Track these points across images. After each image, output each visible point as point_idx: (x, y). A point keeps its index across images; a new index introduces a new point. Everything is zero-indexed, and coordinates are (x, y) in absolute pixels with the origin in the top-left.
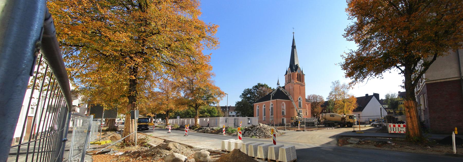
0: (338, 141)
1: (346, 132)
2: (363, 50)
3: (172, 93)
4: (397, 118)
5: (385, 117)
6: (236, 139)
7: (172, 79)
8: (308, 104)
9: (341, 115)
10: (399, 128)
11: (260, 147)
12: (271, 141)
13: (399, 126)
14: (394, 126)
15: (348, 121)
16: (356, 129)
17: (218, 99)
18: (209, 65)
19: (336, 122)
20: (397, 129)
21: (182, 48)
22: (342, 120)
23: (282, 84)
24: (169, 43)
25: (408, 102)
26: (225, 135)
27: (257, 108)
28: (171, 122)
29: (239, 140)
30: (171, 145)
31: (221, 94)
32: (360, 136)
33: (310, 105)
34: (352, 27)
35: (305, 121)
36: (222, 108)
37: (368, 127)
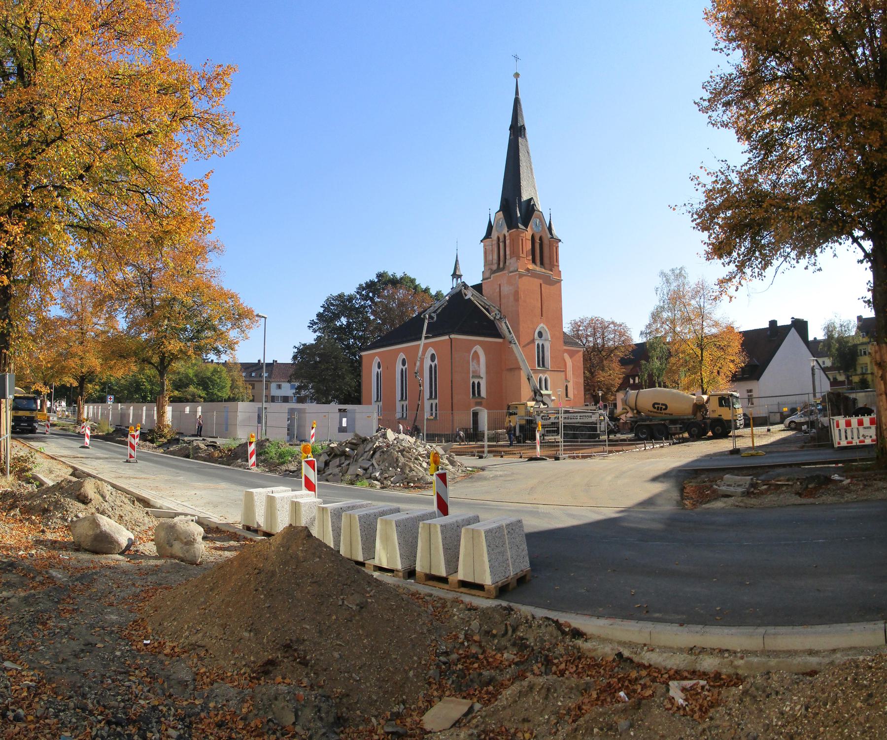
0: (682, 490)
1: (710, 457)
2: (761, 167)
4: (855, 399)
5: (824, 397)
6: (296, 487)
7: (92, 276)
8: (572, 354)
9: (694, 396)
10: (861, 428)
11: (387, 523)
12: (430, 502)
13: (860, 423)
14: (848, 424)
15: (716, 415)
16: (742, 444)
17: (233, 334)
18: (203, 214)
19: (674, 421)
20: (855, 431)
21: (121, 170)
22: (694, 413)
23: (473, 275)
24: (87, 159)
25: (880, 349)
26: (254, 468)
27: (375, 370)
28: (91, 415)
29: (305, 491)
30: (89, 488)
31: (241, 316)
32: (756, 469)
33: (579, 357)
34: (728, 81)
35: (562, 421)
36: (256, 367)
37: (778, 433)
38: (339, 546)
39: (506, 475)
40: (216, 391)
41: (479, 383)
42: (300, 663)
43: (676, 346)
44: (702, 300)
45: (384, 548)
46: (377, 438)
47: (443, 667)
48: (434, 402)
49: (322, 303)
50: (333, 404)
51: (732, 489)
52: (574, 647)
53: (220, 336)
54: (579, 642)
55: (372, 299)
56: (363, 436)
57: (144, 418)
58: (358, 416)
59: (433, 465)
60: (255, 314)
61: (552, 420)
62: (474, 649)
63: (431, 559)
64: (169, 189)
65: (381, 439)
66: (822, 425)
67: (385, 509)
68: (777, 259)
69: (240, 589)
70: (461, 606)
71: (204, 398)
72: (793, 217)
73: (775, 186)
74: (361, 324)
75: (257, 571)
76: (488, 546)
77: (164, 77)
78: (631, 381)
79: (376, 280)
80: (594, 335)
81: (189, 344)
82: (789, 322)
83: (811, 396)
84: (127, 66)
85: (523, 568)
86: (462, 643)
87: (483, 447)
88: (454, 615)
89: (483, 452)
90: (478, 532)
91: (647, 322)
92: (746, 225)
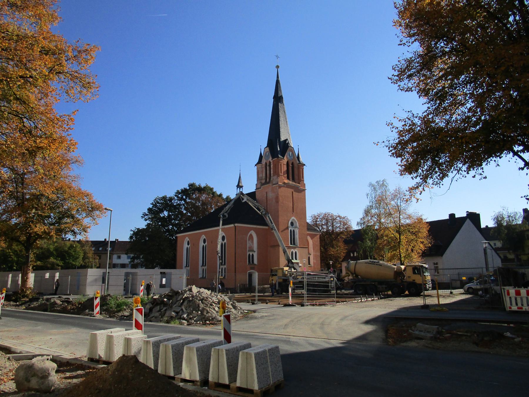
0: (386, 331)
2: (437, 112)
5: (495, 271)
6: (128, 327)
8: (312, 237)
11: (190, 349)
12: (219, 334)
15: (411, 280)
16: (430, 301)
17: (87, 221)
18: (69, 138)
26: (99, 316)
27: (186, 246)
29: (135, 330)
31: (93, 209)
34: (410, 62)
36: (104, 244)
38: (157, 367)
40: (71, 261)
41: (253, 255)
43: (382, 232)
45: (188, 367)
46: (185, 291)
49: (152, 201)
50: (156, 269)
51: (422, 334)
53: (77, 222)
55: (185, 200)
56: (176, 290)
57: (9, 283)
58: (173, 277)
59: (222, 310)
60: (104, 207)
63: (219, 372)
64: (44, 118)
65: (188, 292)
66: (496, 292)
67: (189, 340)
68: (452, 172)
71: (61, 266)
72: (462, 143)
73: (448, 124)
74: (177, 216)
75: (97, 391)
77: (45, 43)
78: (352, 255)
79: (188, 188)
80: (327, 224)
81: (52, 227)
82: (464, 215)
83: (485, 270)
84: (16, 28)
87: (254, 296)
89: (255, 300)
90: (250, 354)
91: (361, 216)
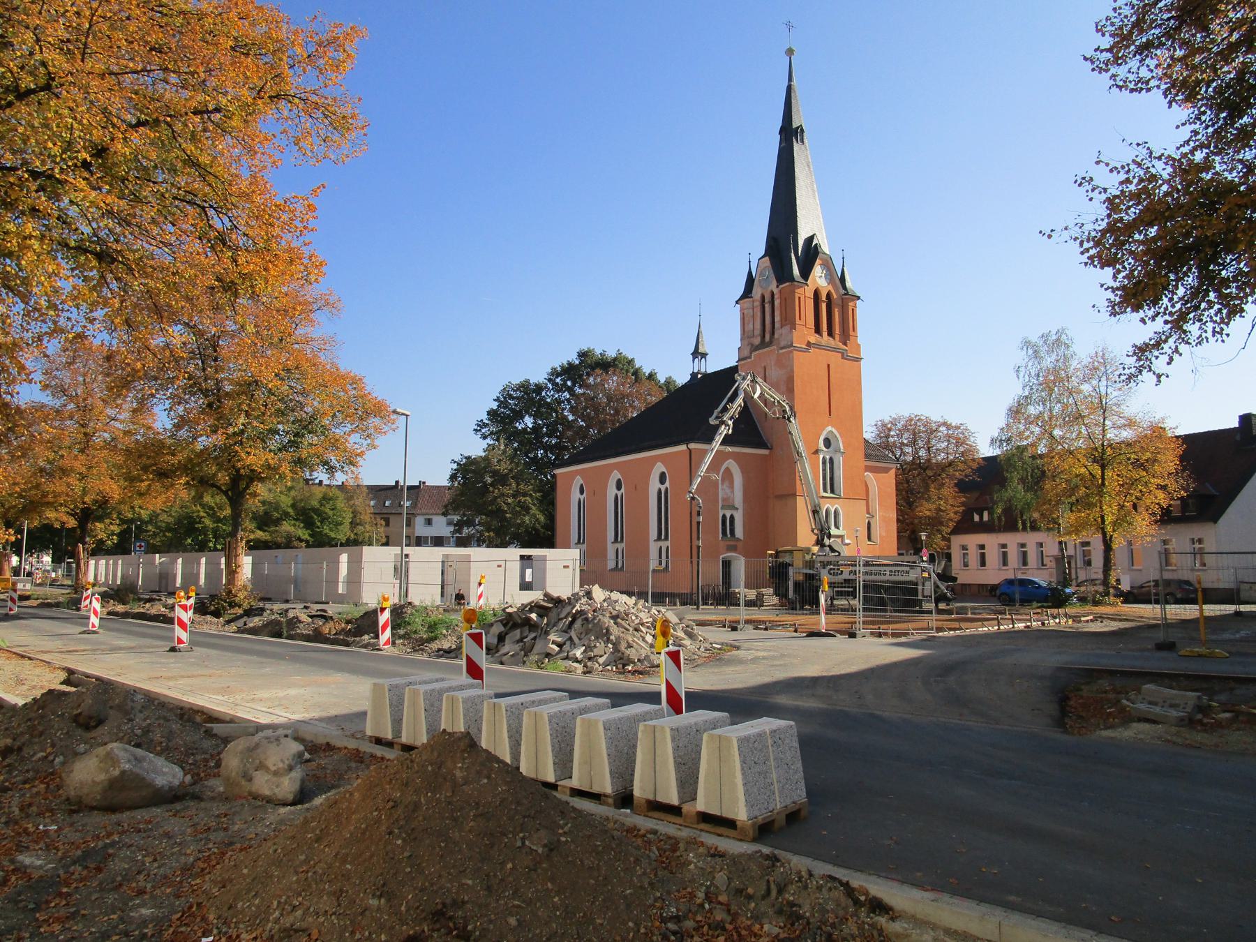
2: (1218, 142)
3: (110, 412)
18: (306, 251)
23: (723, 355)
27: (575, 496)
28: (102, 579)
31: (368, 412)
33: (890, 478)
35: (861, 579)
36: (379, 492)
39: (773, 658)
40: (326, 529)
41: (732, 517)
42: (457, 936)
44: (1104, 382)
47: (673, 938)
48: (664, 544)
49: (496, 394)
51: (1158, 709)
52: (873, 926)
54: (882, 920)
55: (570, 390)
61: (846, 576)
62: (719, 915)
69: (363, 833)
70: (701, 850)
71: (307, 542)
75: (391, 804)
76: (743, 762)
78: (976, 518)
80: (913, 443)
85: (796, 799)
86: (702, 905)
88: (690, 863)
90: (728, 740)
91: (1003, 424)
92: (1189, 248)
